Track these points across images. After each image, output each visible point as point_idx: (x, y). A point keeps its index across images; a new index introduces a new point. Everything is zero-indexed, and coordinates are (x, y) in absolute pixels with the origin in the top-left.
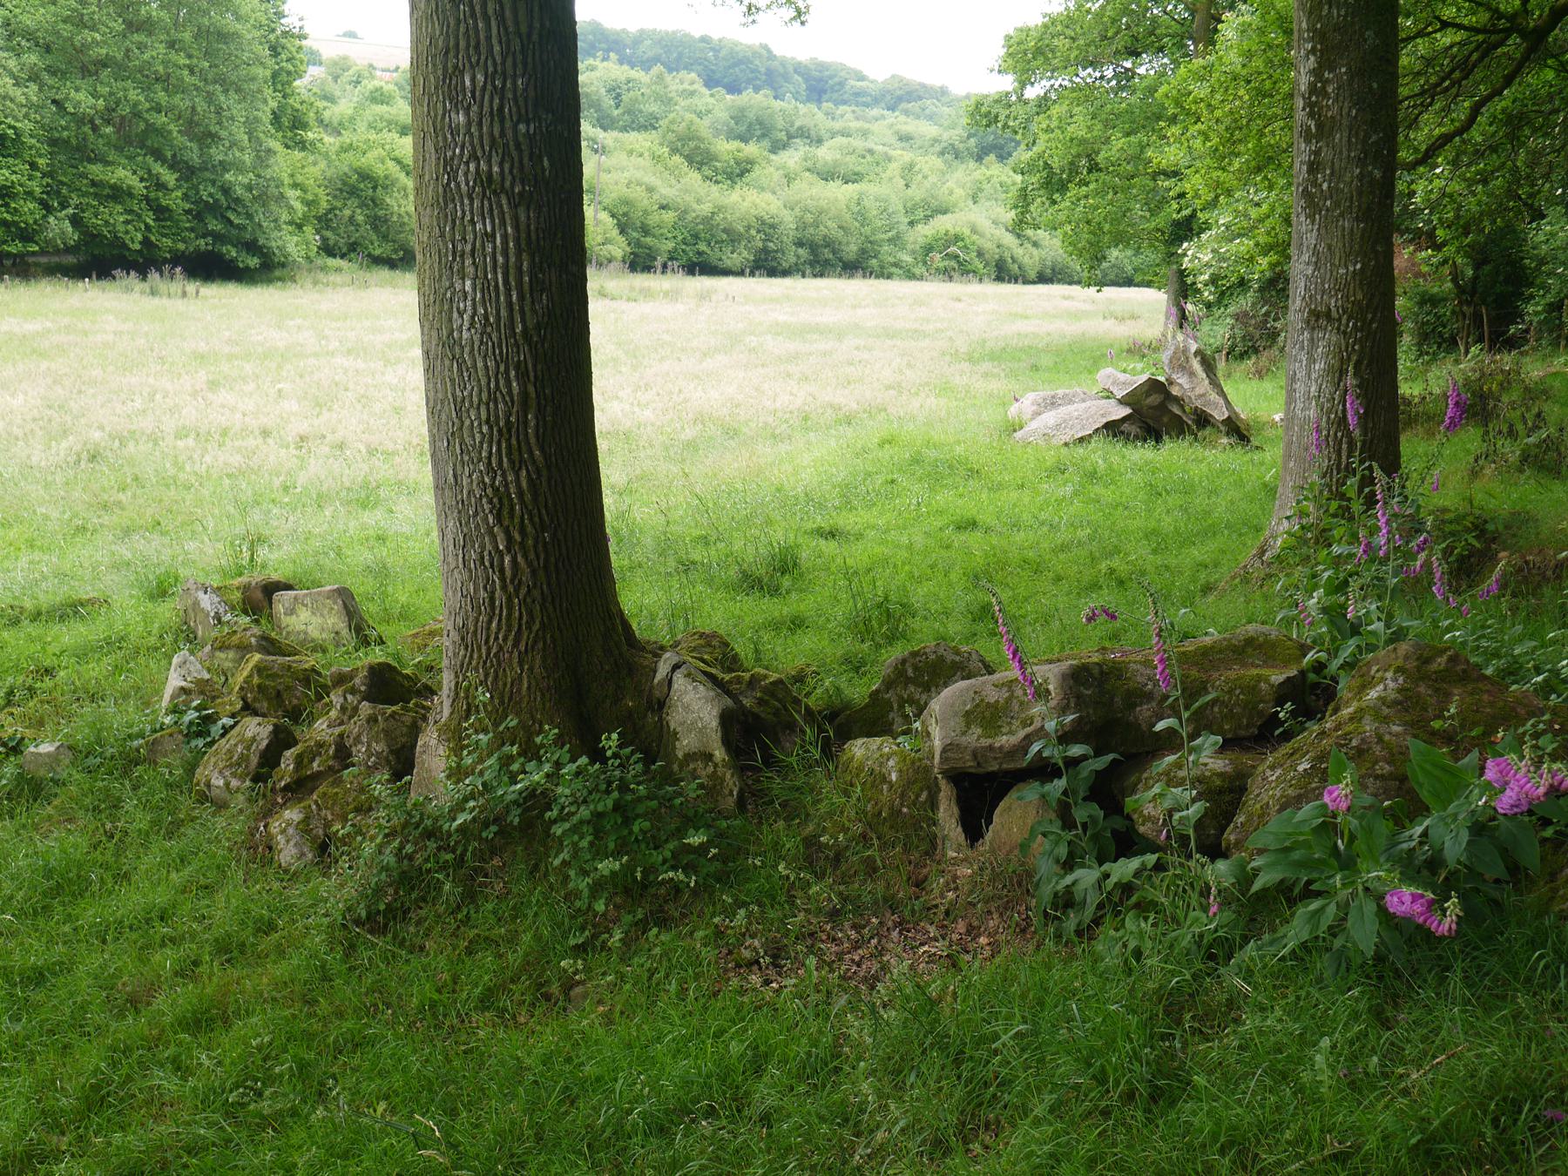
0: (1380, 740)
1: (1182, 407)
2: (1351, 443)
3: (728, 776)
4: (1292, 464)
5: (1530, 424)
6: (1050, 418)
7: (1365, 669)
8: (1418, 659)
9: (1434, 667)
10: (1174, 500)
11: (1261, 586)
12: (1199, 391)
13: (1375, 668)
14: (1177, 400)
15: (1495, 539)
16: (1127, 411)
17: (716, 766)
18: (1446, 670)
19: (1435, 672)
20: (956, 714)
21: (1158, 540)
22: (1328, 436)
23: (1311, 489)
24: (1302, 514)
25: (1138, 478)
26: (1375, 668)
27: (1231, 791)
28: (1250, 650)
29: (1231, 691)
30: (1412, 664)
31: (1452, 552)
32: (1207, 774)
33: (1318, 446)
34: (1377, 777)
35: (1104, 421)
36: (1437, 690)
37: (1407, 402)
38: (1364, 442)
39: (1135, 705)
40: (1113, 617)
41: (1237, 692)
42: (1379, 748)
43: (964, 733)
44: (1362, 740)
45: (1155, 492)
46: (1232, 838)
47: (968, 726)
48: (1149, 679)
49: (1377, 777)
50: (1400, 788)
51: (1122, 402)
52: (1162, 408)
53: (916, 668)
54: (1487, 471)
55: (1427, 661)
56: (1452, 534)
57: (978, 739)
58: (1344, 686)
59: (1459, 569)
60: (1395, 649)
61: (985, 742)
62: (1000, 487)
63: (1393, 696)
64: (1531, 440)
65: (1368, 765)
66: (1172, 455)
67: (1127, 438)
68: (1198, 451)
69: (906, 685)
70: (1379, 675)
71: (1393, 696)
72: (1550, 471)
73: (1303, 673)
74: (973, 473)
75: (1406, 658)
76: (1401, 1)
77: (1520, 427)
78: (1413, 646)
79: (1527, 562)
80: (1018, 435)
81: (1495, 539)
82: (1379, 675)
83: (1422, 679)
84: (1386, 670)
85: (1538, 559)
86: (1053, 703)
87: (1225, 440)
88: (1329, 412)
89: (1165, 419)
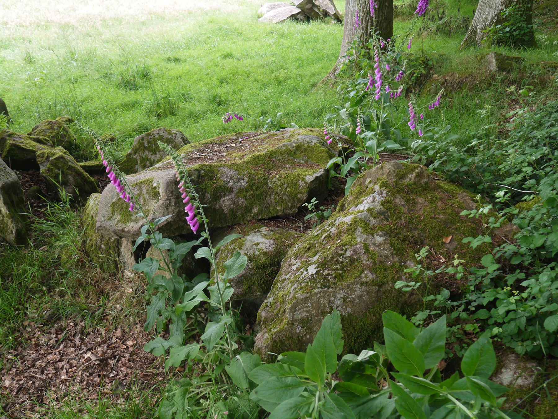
0: (367, 250)
1: (319, 9)
2: (372, 23)
3: (10, 222)
4: (347, 32)
5: (440, 16)
6: (272, 13)
7: (362, 179)
8: (397, 175)
9: (406, 181)
10: (310, 45)
11: (332, 87)
12: (325, 3)
13: (368, 180)
14: (317, 6)
15: (432, 68)
16: (299, 10)
17: (3, 216)
18: (415, 183)
19: (407, 186)
20: (107, 204)
21: (300, 63)
22: (362, 19)
23: (354, 44)
24: (350, 55)
25: (299, 36)
26: (368, 180)
27: (271, 265)
28: (298, 153)
29: (282, 185)
30: (392, 180)
31: (413, 75)
32: (257, 253)
33: (357, 24)
34: (362, 284)
35: (291, 14)
36: (408, 201)
37: (396, 8)
38: (378, 22)
39: (220, 197)
40: (241, 119)
41: (286, 186)
42: (365, 258)
43: (109, 219)
44: (354, 251)
45: (304, 42)
46: (263, 314)
47: (113, 213)
48: (231, 179)
49: (362, 284)
50: (379, 290)
51: (298, 7)
52: (311, 9)
53: (149, 142)
54: (424, 34)
55: (403, 177)
56: (414, 66)
57: (117, 223)
58: (350, 187)
59: (416, 83)
60: (382, 167)
61: (121, 226)
62: (249, 39)
63: (378, 207)
64: (441, 22)
65: (357, 274)
66: (314, 27)
67: (297, 20)
68: (323, 26)
69: (144, 151)
70: (370, 186)
71: (378, 208)
72: (447, 34)
73: (327, 171)
74: (240, 34)
75: (389, 175)
76: (395, 3)
77: (436, 17)
78: (393, 166)
79: (446, 80)
80: (260, 19)
81: (432, 68)
82: (370, 186)
83: (398, 192)
84: (375, 183)
85: (451, 79)
86: (160, 202)
87: (333, 22)
88: (363, 8)
89: (313, 14)
